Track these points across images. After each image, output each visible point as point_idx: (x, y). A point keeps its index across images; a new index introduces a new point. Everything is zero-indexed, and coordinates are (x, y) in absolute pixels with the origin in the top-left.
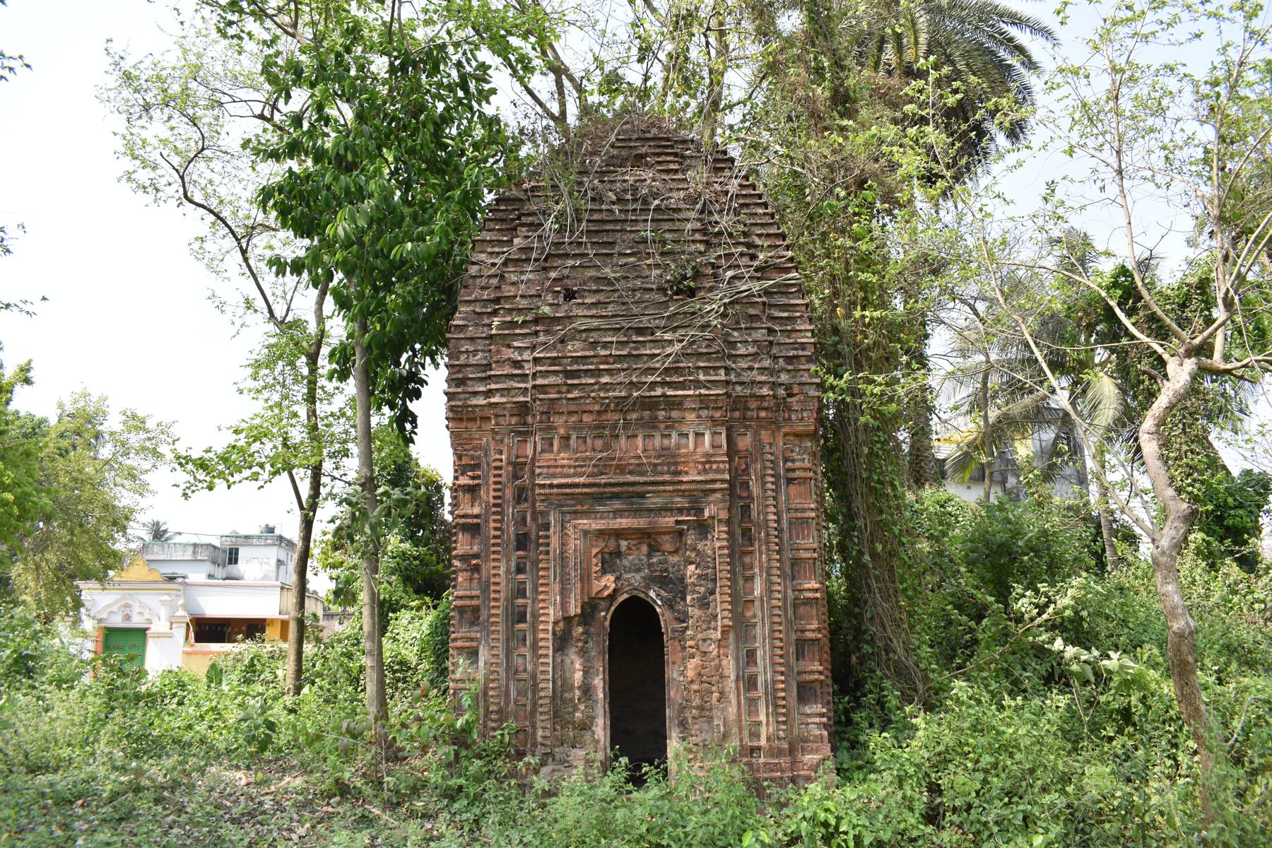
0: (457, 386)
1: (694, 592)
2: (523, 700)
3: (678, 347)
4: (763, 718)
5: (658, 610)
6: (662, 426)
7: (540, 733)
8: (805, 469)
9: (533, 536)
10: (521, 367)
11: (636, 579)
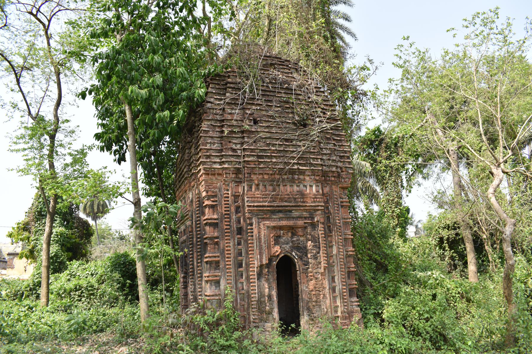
0: (207, 158)
1: (311, 253)
2: (243, 303)
3: (303, 148)
4: (338, 303)
5: (296, 261)
6: (297, 182)
7: (252, 317)
8: (347, 202)
9: (244, 229)
11: (287, 247)
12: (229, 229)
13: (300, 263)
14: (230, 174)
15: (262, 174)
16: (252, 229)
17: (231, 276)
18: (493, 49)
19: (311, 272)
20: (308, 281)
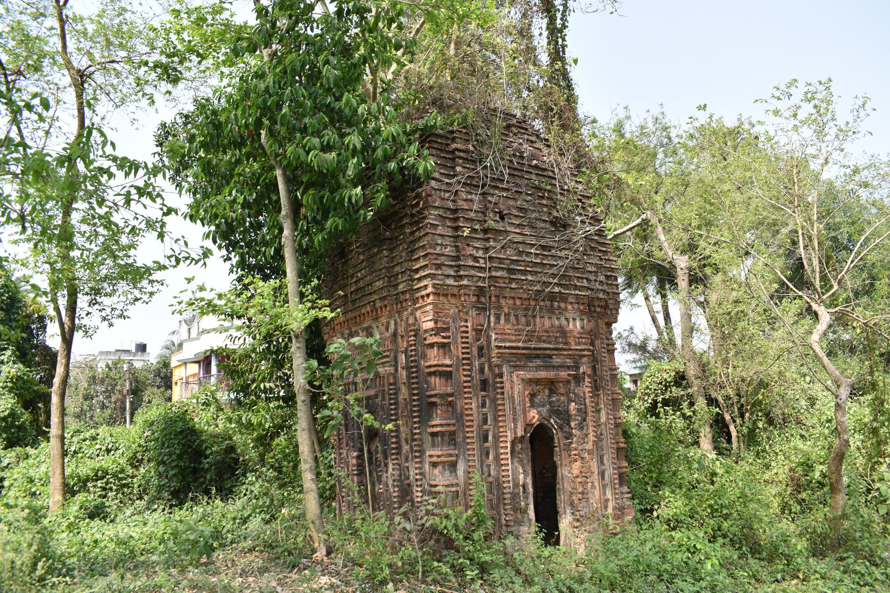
0: (436, 269)
4: (609, 495)
6: (557, 312)
9: (491, 382)
10: (478, 262)
11: (545, 410)
12: (469, 382)
13: (560, 434)
15: (513, 298)
16: (502, 383)
17: (474, 455)
19: (576, 450)
20: (570, 462)
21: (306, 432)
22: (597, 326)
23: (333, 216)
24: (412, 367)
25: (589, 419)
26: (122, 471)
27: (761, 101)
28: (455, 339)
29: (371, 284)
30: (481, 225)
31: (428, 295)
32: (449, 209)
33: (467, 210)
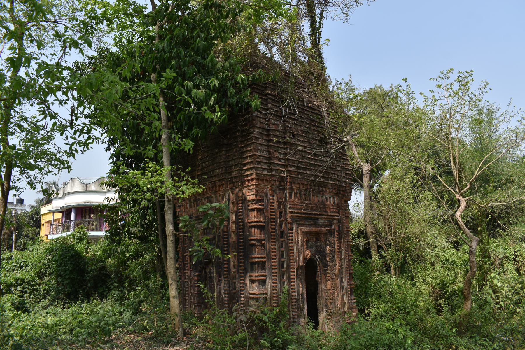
0: (258, 165)
4: (345, 300)
10: (281, 161)
11: (313, 250)
12: (274, 232)
14: (275, 181)
15: (299, 184)
16: (292, 233)
17: (276, 276)
18: (495, 110)
19: (329, 274)
20: (326, 281)
21: (173, 260)
22: (341, 202)
23: (196, 128)
24: (240, 222)
25: (336, 256)
26: (33, 281)
27: (434, 79)
28: (267, 206)
29: (213, 171)
30: (282, 140)
31: (252, 180)
32: (264, 129)
33: (275, 130)
